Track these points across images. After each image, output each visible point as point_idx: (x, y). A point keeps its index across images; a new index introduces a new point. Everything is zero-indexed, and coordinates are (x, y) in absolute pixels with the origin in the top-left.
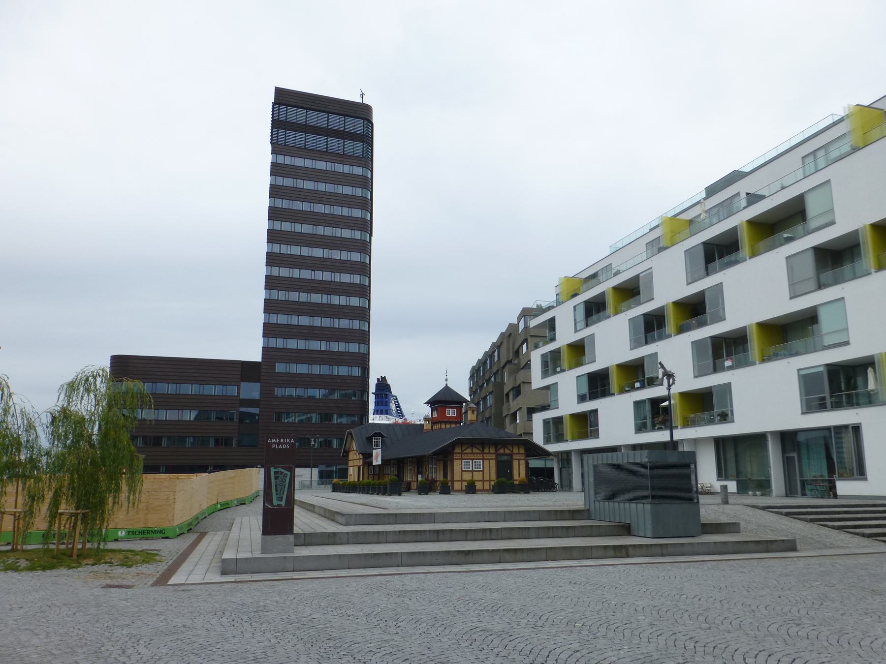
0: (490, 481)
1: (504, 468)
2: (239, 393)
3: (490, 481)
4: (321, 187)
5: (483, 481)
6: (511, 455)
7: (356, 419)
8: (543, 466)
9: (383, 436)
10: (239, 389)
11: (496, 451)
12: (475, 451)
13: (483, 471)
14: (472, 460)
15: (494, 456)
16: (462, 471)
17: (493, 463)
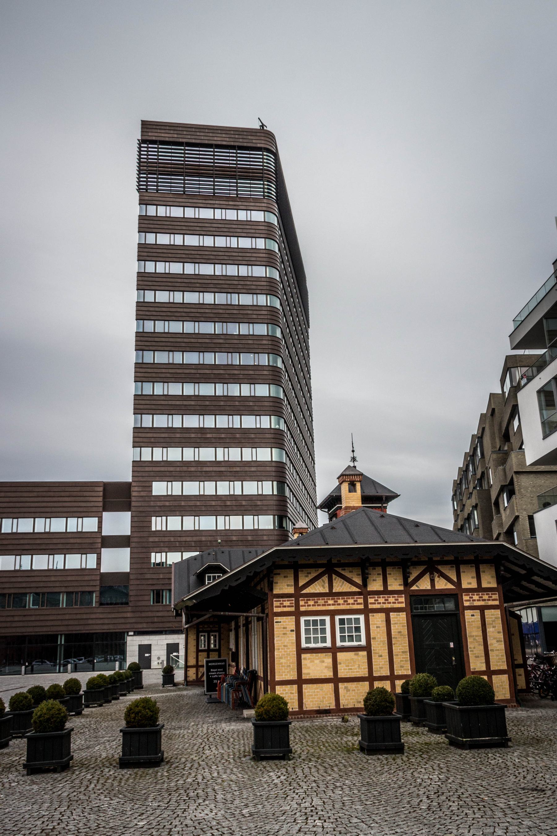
4: (208, 241)
6: (454, 597)
11: (406, 584)
12: (340, 586)
13: (368, 648)
15: (401, 602)
16: (300, 651)
17: (400, 621)
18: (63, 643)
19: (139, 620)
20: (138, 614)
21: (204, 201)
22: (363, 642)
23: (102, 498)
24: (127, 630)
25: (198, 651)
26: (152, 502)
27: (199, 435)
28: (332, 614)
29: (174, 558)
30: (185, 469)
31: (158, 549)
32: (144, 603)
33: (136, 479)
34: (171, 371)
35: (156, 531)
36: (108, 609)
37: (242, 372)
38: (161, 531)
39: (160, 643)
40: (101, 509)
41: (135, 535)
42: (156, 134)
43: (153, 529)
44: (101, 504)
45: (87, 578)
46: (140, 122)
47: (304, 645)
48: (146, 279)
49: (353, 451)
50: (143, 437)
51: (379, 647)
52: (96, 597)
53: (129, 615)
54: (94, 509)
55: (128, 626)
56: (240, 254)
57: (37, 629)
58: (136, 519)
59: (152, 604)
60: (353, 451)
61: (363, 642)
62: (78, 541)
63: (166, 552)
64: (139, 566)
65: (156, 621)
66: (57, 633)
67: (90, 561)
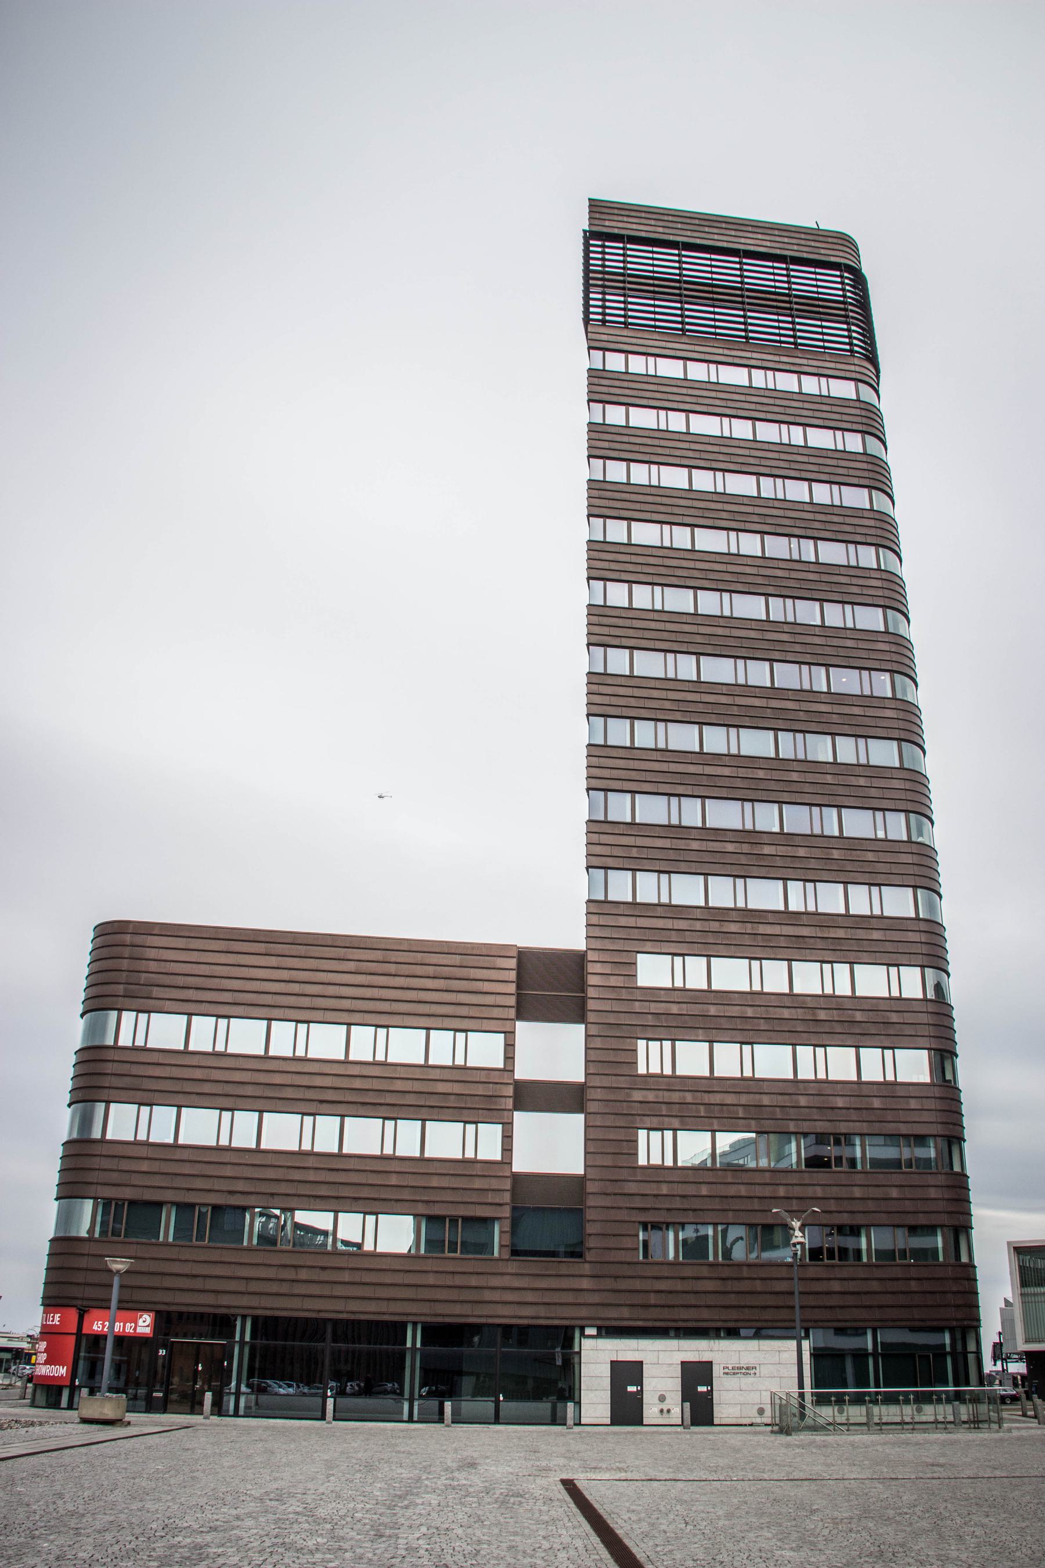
2: (507, 1148)
7: (933, 1154)
10: (507, 1138)
18: (418, 1345)
19: (611, 1298)
20: (608, 1284)
21: (726, 352)
23: (514, 985)
24: (583, 1323)
26: (637, 1003)
27: (746, 848)
29: (694, 1147)
30: (715, 926)
31: (655, 1119)
32: (621, 1256)
33: (598, 944)
34: (672, 695)
35: (649, 1076)
36: (534, 1265)
37: (837, 709)
38: (661, 1076)
39: (664, 1358)
40: (512, 1013)
41: (596, 1081)
42: (620, 225)
43: (642, 1070)
44: (512, 1001)
45: (478, 1184)
46: (587, 204)
48: (608, 494)
50: (611, 846)
52: (501, 1232)
53: (585, 1283)
54: (496, 1012)
55: (584, 1312)
56: (813, 460)
58: (598, 1043)
59: (641, 1258)
62: (457, 1088)
63: (675, 1130)
64: (608, 1161)
65: (652, 1302)
66: (404, 1318)
67: (487, 1142)
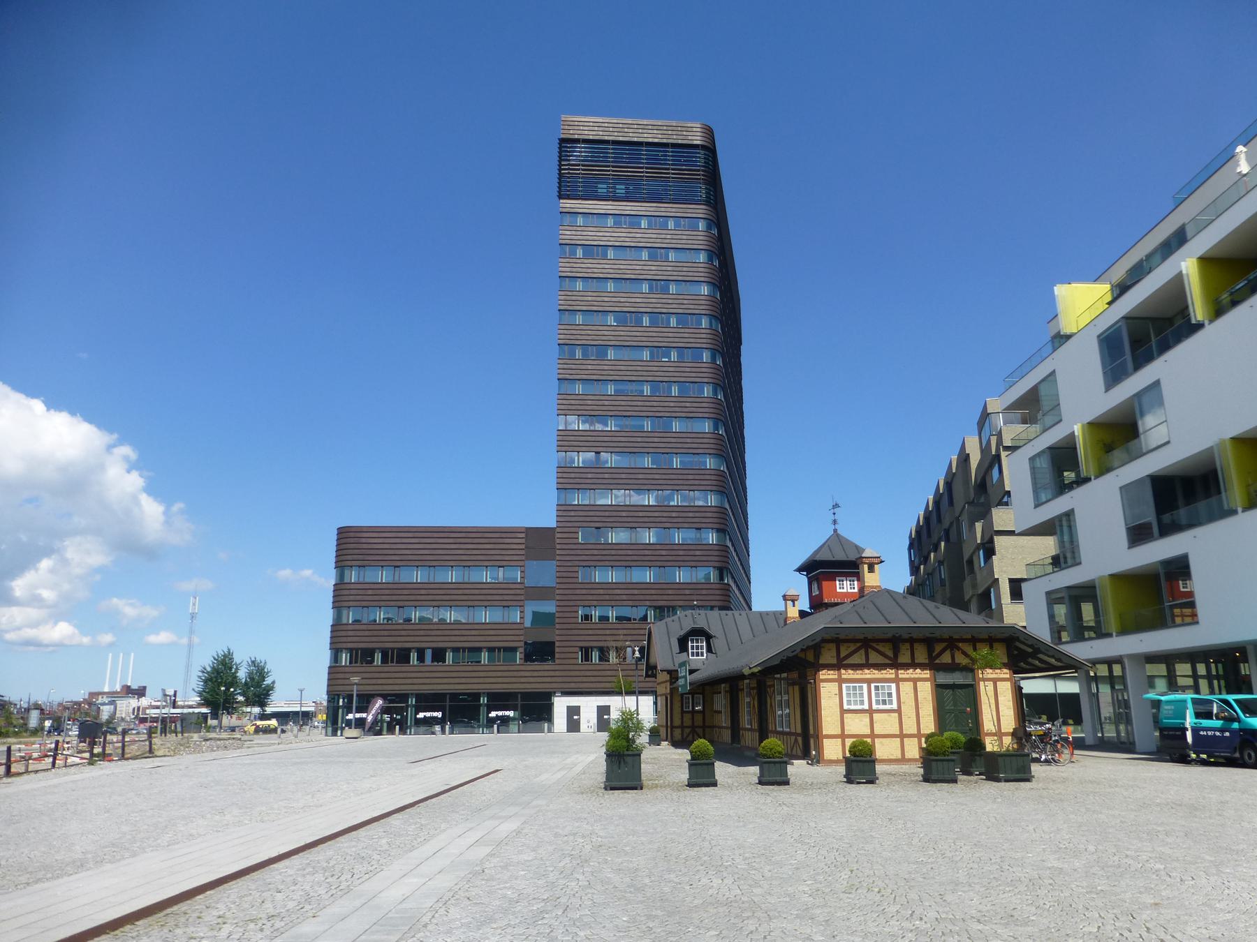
0: (918, 735)
1: (958, 705)
3: (918, 735)
5: (902, 736)
8: (1053, 691)
9: (708, 637)
12: (874, 658)
13: (899, 711)
14: (869, 682)
16: (843, 712)
22: (895, 706)
25: (683, 712)
28: (869, 682)
47: (846, 707)
49: (835, 522)
51: (908, 710)
57: (435, 687)
60: (835, 522)
61: (895, 706)
